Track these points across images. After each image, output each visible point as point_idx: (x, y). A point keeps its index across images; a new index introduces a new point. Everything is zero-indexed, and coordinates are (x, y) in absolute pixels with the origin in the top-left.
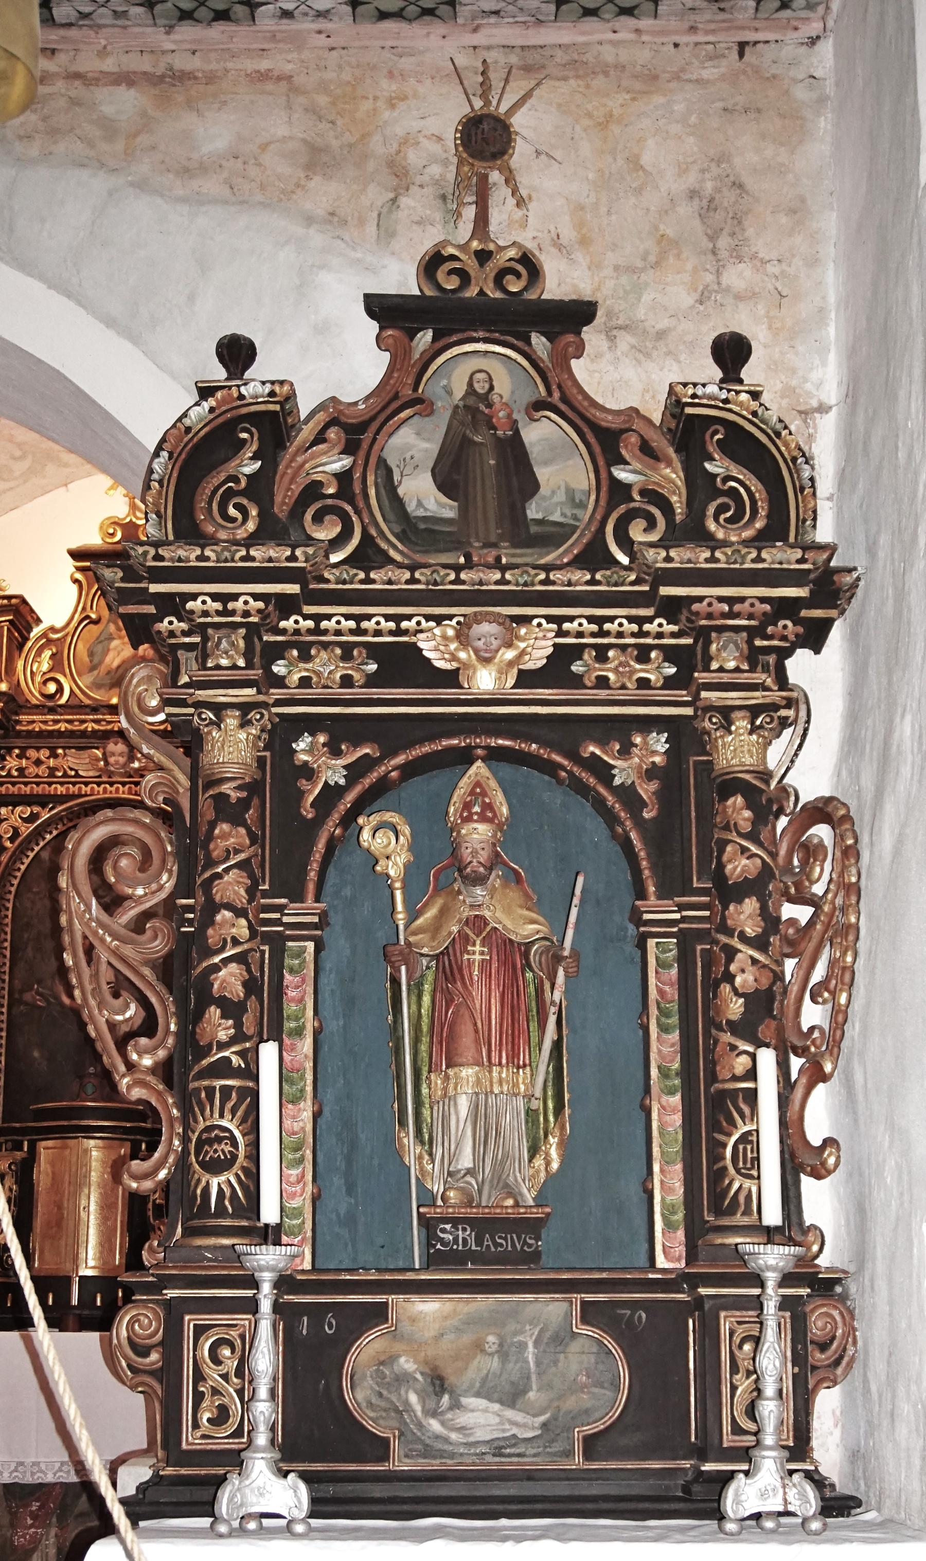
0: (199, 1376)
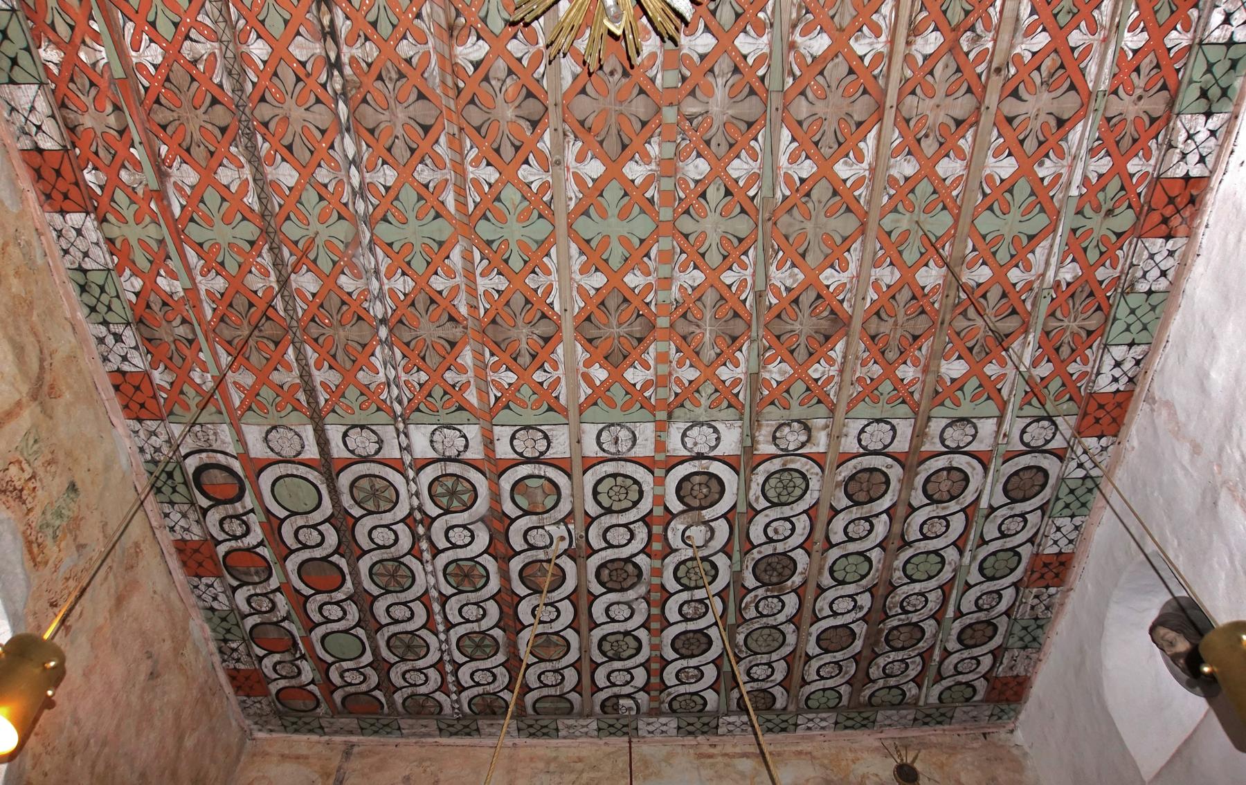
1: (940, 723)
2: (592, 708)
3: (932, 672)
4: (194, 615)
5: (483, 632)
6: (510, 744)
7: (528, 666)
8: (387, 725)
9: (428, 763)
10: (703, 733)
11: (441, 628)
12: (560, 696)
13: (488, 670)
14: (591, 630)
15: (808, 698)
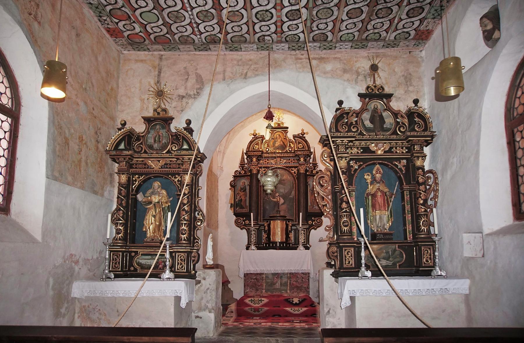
0: (345, 257)
1: (393, 47)
2: (254, 40)
3: (393, 27)
4: (84, 6)
5: (207, 11)
6: (223, 54)
7: (227, 24)
8: (174, 48)
9: (192, 62)
10: (299, 50)
11: (189, 9)
12: (241, 35)
13: (211, 26)
14: (252, 9)
15: (341, 37)
